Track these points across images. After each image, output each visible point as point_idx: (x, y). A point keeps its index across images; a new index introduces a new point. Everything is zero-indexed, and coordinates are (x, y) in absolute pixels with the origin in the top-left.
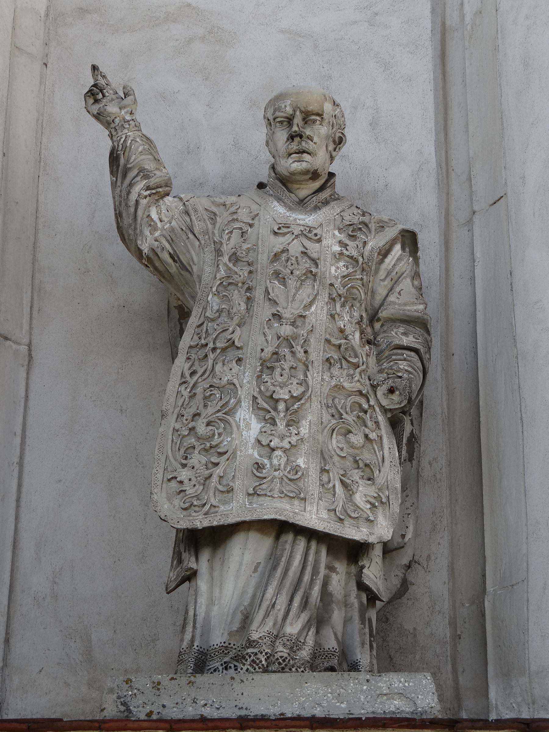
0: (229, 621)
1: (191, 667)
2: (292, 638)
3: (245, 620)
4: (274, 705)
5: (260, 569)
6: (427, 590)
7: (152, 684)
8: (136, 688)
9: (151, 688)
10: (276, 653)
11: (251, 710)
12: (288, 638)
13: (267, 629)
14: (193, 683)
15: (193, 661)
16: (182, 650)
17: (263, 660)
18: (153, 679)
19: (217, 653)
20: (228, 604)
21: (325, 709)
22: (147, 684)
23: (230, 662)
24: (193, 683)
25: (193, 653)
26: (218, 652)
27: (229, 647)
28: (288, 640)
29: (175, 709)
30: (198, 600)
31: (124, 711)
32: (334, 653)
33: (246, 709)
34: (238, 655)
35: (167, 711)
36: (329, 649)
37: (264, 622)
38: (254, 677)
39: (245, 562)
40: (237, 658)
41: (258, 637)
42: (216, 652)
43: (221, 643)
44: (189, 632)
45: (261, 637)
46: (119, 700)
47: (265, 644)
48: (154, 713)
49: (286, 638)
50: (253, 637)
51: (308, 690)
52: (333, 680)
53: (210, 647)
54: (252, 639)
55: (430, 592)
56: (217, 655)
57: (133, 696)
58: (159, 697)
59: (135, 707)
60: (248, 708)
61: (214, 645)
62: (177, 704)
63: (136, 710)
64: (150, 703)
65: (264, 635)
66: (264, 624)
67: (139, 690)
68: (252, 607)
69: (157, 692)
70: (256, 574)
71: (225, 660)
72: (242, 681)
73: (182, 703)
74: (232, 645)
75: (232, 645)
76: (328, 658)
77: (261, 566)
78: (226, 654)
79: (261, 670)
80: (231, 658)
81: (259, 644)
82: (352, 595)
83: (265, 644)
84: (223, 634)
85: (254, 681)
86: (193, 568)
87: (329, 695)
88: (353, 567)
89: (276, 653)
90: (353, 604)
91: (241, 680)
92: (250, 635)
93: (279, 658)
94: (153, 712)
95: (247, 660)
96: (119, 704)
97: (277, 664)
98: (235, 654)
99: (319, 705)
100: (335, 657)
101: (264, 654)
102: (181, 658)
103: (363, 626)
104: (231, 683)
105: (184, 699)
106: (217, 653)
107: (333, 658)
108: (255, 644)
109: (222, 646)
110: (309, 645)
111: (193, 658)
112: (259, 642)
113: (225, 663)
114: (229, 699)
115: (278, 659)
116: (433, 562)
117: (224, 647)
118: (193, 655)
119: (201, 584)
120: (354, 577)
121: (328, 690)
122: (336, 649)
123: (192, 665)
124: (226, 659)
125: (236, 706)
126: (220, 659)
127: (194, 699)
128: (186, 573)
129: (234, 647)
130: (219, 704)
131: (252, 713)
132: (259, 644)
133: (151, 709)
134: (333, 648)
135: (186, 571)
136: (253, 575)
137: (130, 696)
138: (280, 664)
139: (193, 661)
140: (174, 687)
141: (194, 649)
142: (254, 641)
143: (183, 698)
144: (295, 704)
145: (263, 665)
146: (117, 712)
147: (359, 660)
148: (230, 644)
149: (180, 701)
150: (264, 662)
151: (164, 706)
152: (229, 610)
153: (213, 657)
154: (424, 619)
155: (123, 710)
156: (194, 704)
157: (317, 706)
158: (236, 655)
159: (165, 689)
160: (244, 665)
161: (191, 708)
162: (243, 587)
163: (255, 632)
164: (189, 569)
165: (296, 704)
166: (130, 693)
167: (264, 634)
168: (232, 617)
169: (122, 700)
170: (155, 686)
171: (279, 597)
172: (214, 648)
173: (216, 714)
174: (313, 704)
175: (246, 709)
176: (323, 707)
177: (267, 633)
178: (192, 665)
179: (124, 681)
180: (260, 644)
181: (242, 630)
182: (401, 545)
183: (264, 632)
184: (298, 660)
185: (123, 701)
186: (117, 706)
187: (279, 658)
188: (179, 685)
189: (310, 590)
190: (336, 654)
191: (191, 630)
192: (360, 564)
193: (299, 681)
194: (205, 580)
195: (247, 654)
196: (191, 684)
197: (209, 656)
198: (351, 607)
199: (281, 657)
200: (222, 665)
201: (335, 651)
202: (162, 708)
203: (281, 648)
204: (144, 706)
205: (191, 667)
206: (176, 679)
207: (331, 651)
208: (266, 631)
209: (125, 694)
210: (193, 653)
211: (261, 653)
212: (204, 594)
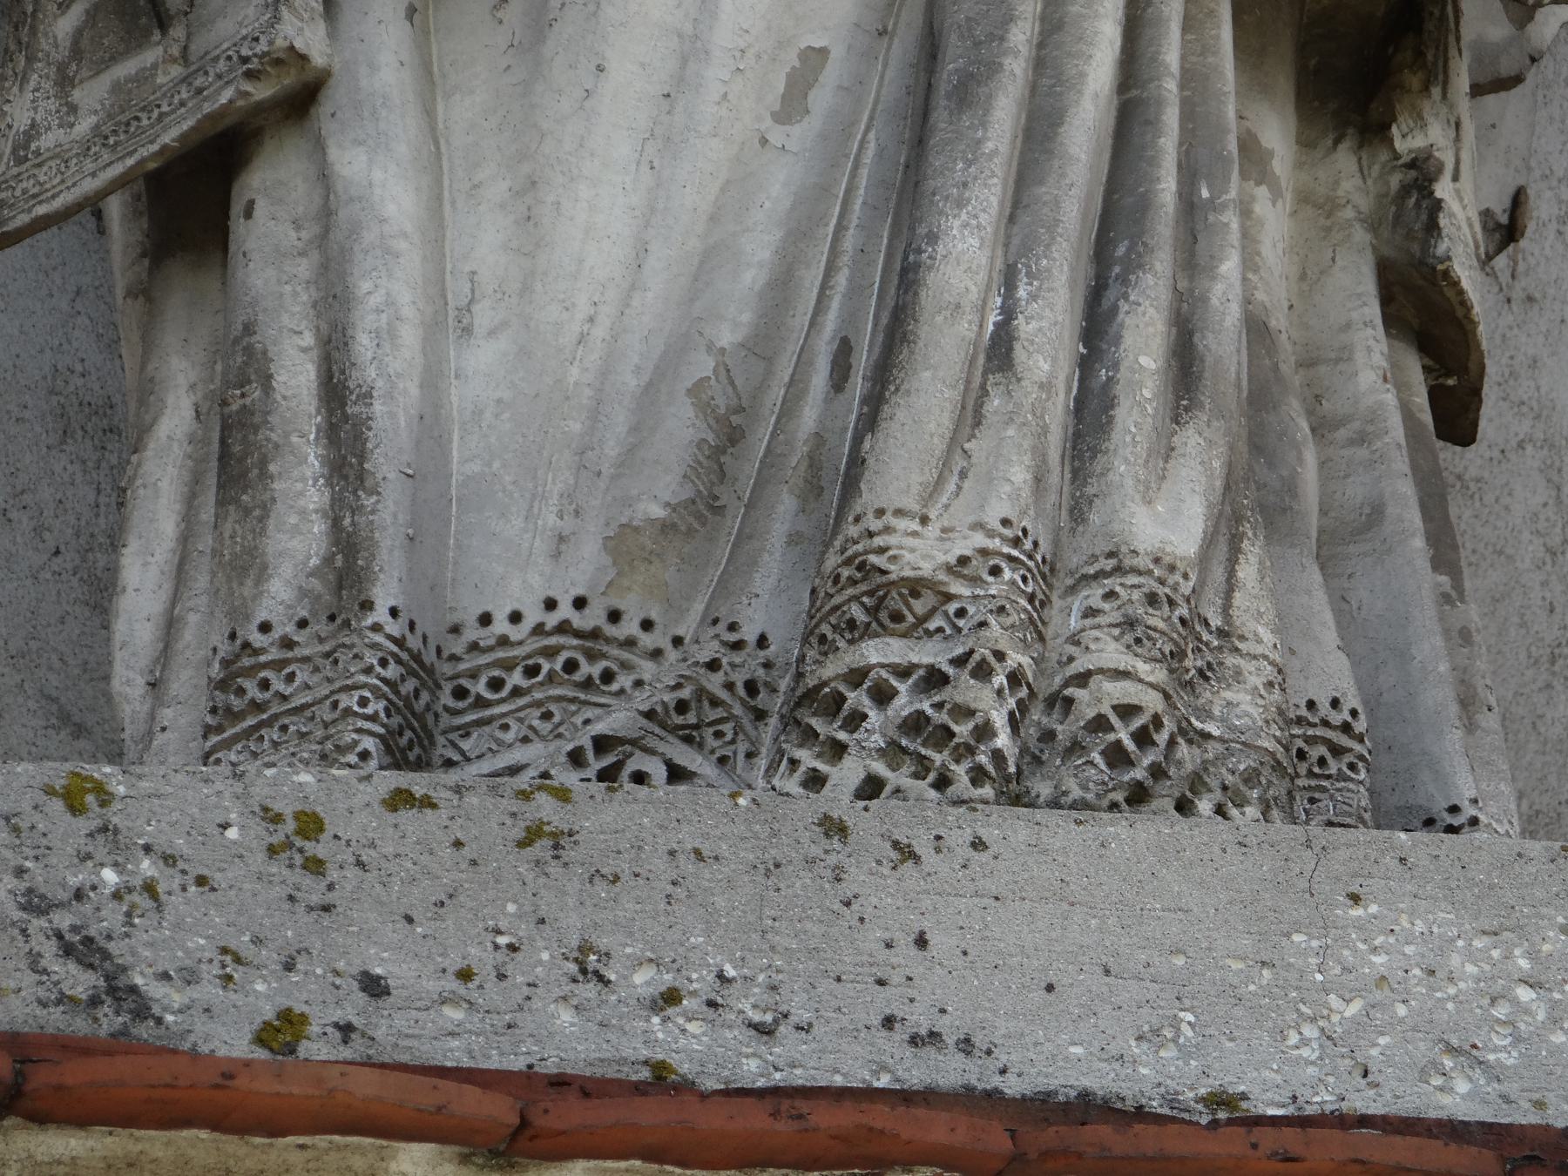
0: (612, 450)
1: (364, 756)
2: (1175, 588)
3: (719, 451)
4: (1156, 1032)
5: (822, 98)
6: (1524, 428)
7: (258, 828)
8: (147, 849)
9: (261, 856)
10: (1083, 679)
11: (1003, 1058)
12: (1151, 584)
13: (1005, 510)
14: (559, 840)
15: (373, 718)
16: (258, 639)
17: (999, 719)
18: (260, 792)
19: (516, 678)
20: (600, 332)
21: (1512, 1088)
22: (225, 826)
23: (634, 742)
24: (559, 840)
25: (371, 659)
26: (532, 671)
27: (608, 640)
28: (1152, 599)
29: (454, 1014)
30: (366, 286)
31: (94, 1002)
32: (1345, 741)
33: (966, 1045)
34: (701, 693)
35: (401, 1021)
36: (1311, 705)
37: (959, 462)
38: (984, 833)
39: (724, 36)
40: (691, 718)
41: (941, 558)
42: (509, 666)
43: (551, 605)
44: (303, 513)
45: (963, 561)
46: (37, 924)
47: (1002, 609)
48: (314, 1029)
49: (1133, 580)
50: (908, 556)
51: (1374, 950)
52: (1539, 893)
53: (455, 630)
54: (896, 571)
55: (1548, 443)
56: (517, 692)
57: (135, 898)
58: (326, 920)
59: (165, 976)
60: (979, 1040)
61: (486, 620)
62: (465, 975)
63: (178, 999)
64: (269, 956)
65: (984, 552)
66: (963, 475)
67: (169, 860)
68: (769, 360)
69: (308, 881)
70: (796, 130)
71: (599, 728)
72: (907, 853)
73: (502, 977)
74: (630, 627)
75: (630, 627)
76: (1311, 774)
77: (832, 74)
78: (587, 684)
79: (987, 791)
80: (650, 715)
81: (952, 608)
82: (1360, 357)
83: (1002, 609)
84: (562, 539)
85: (984, 857)
86: (304, 58)
87: (1525, 994)
88: (1345, 160)
89: (1083, 679)
90: (1374, 416)
91: (896, 845)
92: (878, 541)
93: (1114, 719)
94: (304, 1019)
95: (855, 720)
96: (49, 948)
97: (1096, 757)
98: (678, 686)
99: (1468, 1054)
100: (1352, 767)
101: (1000, 679)
102: (253, 691)
103: (1444, 579)
104: (832, 859)
105: (513, 948)
106: (516, 678)
107: (1341, 777)
108: (919, 606)
109: (564, 628)
110: (1259, 650)
111: (374, 690)
112: (949, 597)
113: (602, 744)
114: (835, 970)
115: (1100, 724)
116: (1552, 236)
117: (578, 634)
118: (368, 670)
119: (377, 175)
120: (1361, 236)
121: (1507, 957)
122: (1354, 713)
123: (369, 743)
124: (617, 720)
125: (889, 1022)
126: (547, 716)
127: (585, 948)
128: (247, 87)
129: (647, 640)
130: (769, 999)
131: (1011, 1078)
132: (952, 608)
133: (285, 1003)
134: (1335, 703)
135: (250, 75)
136: (777, 136)
137: (117, 896)
138: (1117, 757)
139: (373, 718)
140: (425, 859)
141: (376, 628)
142: (915, 587)
143: (502, 940)
144: (1293, 1038)
145: (998, 756)
146: (43, 1004)
147: (1469, 811)
148: (615, 616)
149: (481, 957)
150: (1003, 740)
151: (374, 987)
152: (605, 372)
153: (481, 703)
154: (1523, 625)
155: (81, 992)
156: (589, 990)
157: (1448, 1063)
158: (685, 693)
159: (360, 864)
160: (837, 750)
161: (566, 1016)
162: (713, 219)
163: (915, 526)
164: (278, 62)
165: (1304, 1042)
166: (110, 876)
167: (980, 540)
168: (635, 429)
169: (63, 920)
170: (289, 845)
171: (1033, 297)
172: (486, 636)
173: (753, 1065)
174: (1422, 1049)
175: (966, 1045)
176: (1495, 1074)
177: (1004, 539)
178: (369, 743)
179: (50, 791)
180: (961, 613)
181: (699, 517)
182: (1506, 68)
183: (978, 526)
184: (1220, 747)
185: (74, 929)
186: (34, 960)
187: (1114, 719)
188: (458, 844)
189: (1191, 278)
190: (1357, 747)
191: (315, 497)
192: (1406, 142)
193: (1303, 884)
194: (402, 149)
195: (856, 677)
196: (541, 848)
197: (446, 699)
198: (1361, 439)
199: (1127, 711)
200: (576, 758)
201: (1346, 728)
202: (361, 998)
203: (1110, 652)
204: (229, 978)
205: (364, 756)
206: (428, 803)
207: (1325, 723)
208: (993, 520)
209: (74, 881)
210: (371, 659)
211: (983, 672)
212: (402, 245)
